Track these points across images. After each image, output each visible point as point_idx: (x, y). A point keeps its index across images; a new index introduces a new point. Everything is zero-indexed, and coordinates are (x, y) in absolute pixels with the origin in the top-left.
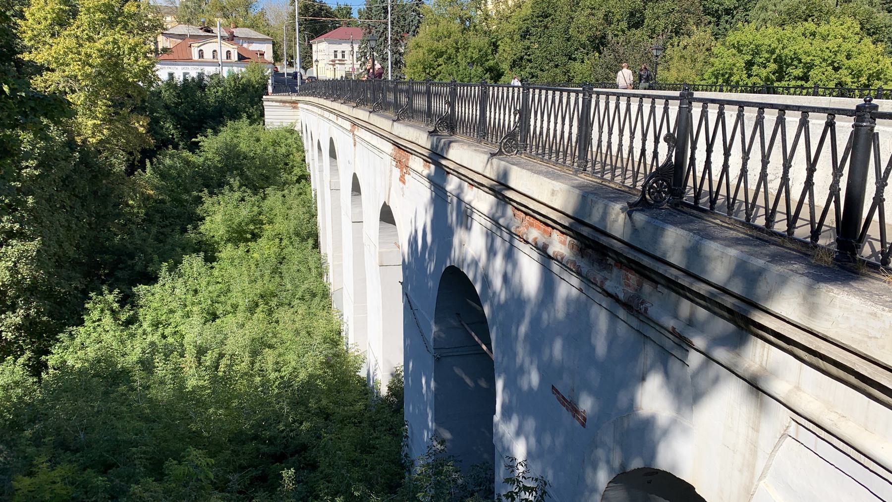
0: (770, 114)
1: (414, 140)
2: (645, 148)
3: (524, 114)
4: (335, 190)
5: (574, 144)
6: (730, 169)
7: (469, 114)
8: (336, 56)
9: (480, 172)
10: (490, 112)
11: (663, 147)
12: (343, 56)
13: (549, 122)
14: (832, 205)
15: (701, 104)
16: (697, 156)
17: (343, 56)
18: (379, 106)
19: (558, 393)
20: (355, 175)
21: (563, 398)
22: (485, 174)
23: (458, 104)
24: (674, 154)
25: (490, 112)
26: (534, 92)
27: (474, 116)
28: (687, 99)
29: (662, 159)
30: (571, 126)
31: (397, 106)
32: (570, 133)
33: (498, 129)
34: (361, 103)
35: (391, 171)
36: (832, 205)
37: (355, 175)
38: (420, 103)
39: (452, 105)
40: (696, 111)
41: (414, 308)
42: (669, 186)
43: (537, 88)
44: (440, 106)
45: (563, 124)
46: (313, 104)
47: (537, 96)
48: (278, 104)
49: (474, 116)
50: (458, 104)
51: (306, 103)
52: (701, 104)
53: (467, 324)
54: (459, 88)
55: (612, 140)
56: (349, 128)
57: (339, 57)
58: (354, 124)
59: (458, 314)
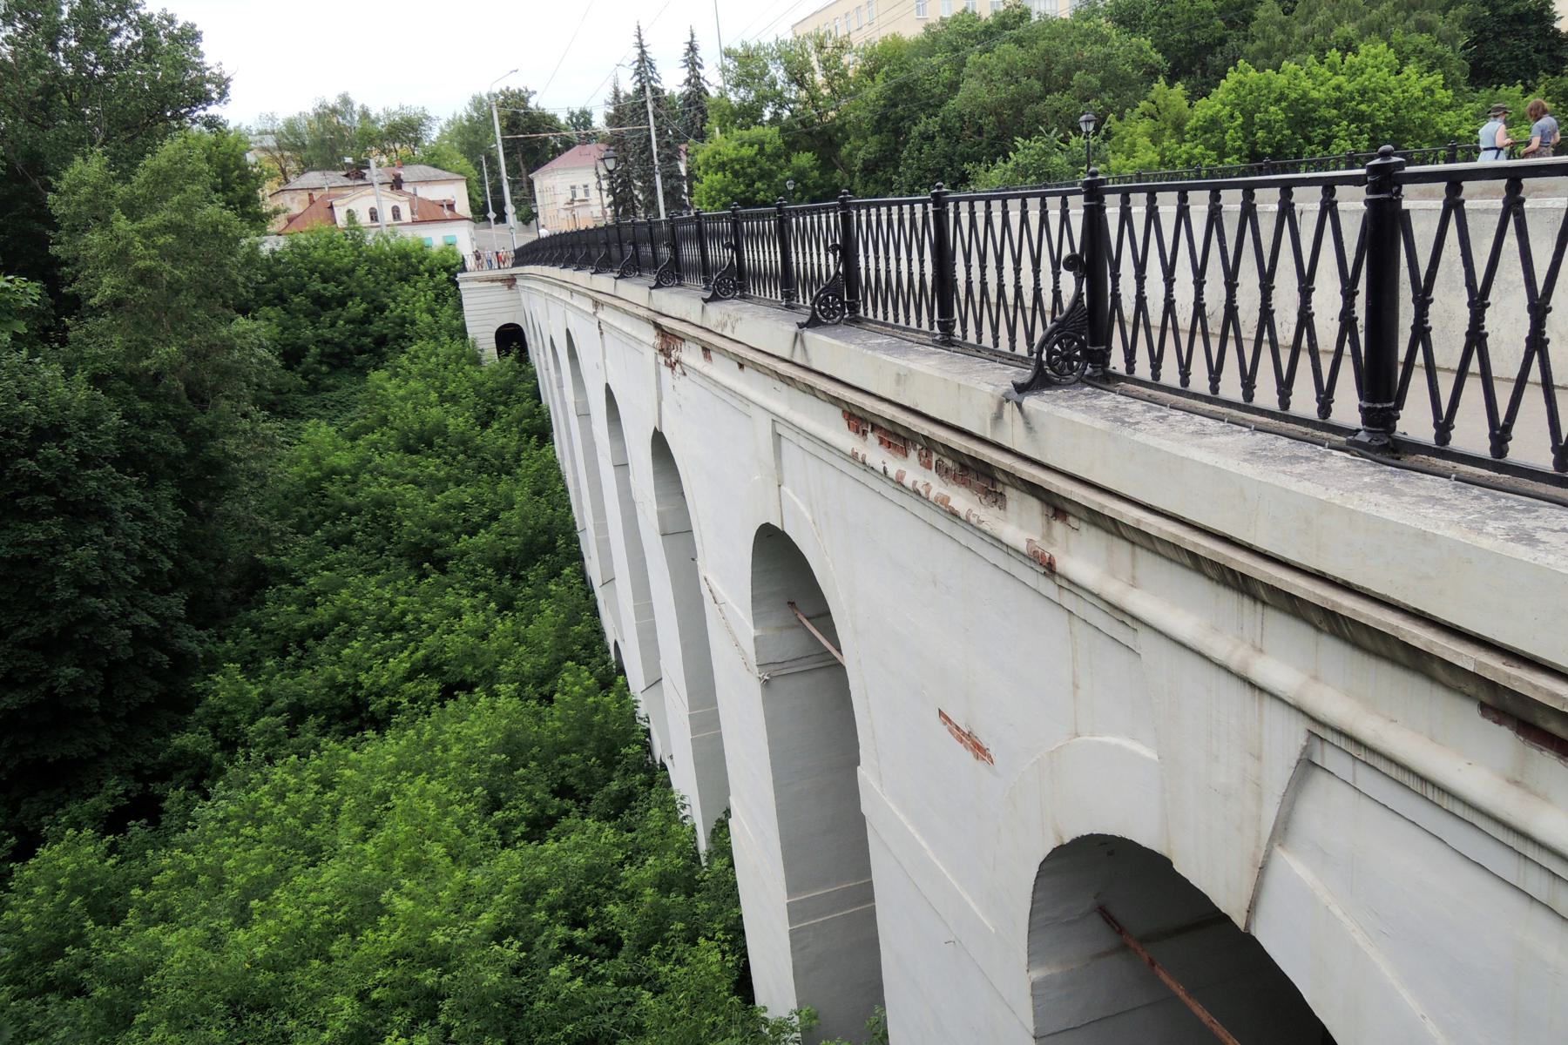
0: (1483, 194)
1: (683, 317)
2: (1302, 295)
3: (847, 252)
4: (584, 415)
5: (930, 293)
6: (1177, 305)
7: (805, 264)
8: (574, 194)
9: (787, 357)
10: (867, 258)
11: (1068, 280)
12: (587, 192)
13: (910, 261)
14: (1347, 348)
15: (1502, 183)
16: (1121, 289)
17: (587, 192)
18: (629, 268)
19: (950, 721)
20: (607, 385)
21: (958, 728)
22: (795, 360)
23: (796, 248)
24: (1084, 289)
25: (867, 258)
26: (957, 207)
27: (809, 265)
28: (1094, 193)
29: (1067, 299)
30: (922, 262)
31: (705, 268)
32: (922, 275)
33: (811, 281)
34: (602, 266)
35: (658, 374)
36: (1347, 348)
37: (607, 385)
38: (763, 255)
39: (737, 249)
40: (1112, 212)
41: (719, 601)
42: (1082, 345)
43: (980, 198)
44: (719, 254)
45: (983, 268)
46: (562, 284)
47: (864, 218)
48: (489, 284)
49: (809, 265)
50: (796, 248)
51: (544, 280)
52: (1502, 183)
53: (808, 619)
54: (794, 220)
55: (1022, 282)
56: (591, 310)
57: (580, 195)
58: (596, 304)
59: (792, 604)
